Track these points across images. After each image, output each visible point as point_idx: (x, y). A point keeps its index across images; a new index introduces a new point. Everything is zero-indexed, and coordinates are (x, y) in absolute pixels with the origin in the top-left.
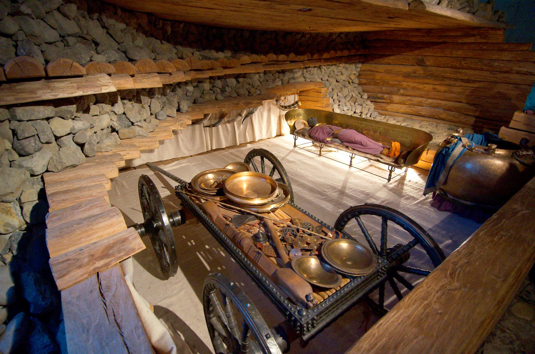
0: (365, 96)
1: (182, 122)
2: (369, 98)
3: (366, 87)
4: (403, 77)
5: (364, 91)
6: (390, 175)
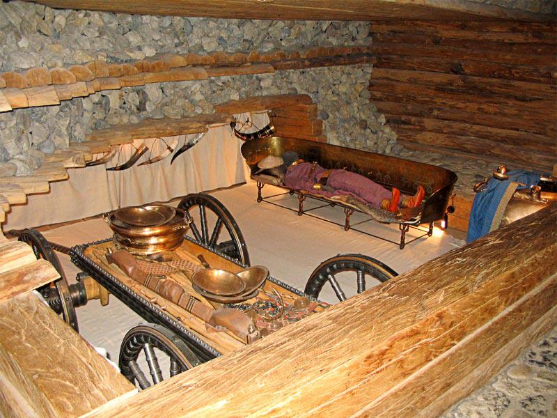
0: (383, 119)
1: (78, 156)
2: (388, 122)
3: (382, 105)
4: (436, 90)
5: (380, 111)
6: (403, 238)
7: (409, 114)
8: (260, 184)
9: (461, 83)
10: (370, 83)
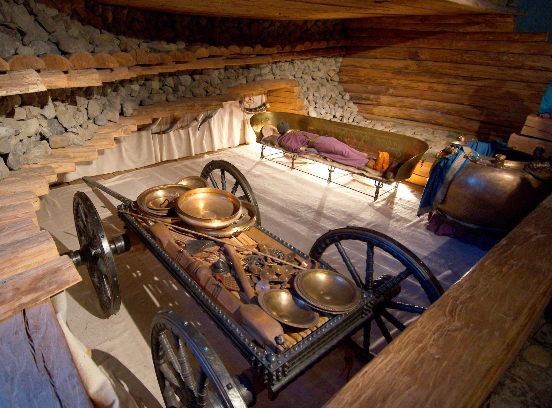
0: (347, 97)
1: (126, 127)
2: (351, 98)
4: (393, 73)
5: (345, 91)
6: (377, 192)
7: (369, 93)
8: (263, 146)
9: (415, 67)
10: (339, 69)
